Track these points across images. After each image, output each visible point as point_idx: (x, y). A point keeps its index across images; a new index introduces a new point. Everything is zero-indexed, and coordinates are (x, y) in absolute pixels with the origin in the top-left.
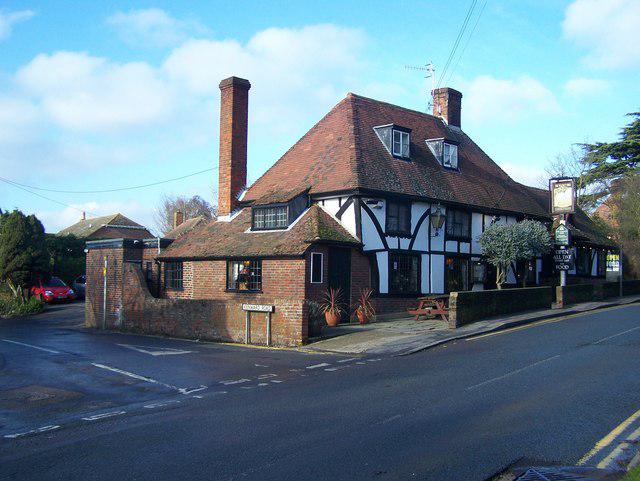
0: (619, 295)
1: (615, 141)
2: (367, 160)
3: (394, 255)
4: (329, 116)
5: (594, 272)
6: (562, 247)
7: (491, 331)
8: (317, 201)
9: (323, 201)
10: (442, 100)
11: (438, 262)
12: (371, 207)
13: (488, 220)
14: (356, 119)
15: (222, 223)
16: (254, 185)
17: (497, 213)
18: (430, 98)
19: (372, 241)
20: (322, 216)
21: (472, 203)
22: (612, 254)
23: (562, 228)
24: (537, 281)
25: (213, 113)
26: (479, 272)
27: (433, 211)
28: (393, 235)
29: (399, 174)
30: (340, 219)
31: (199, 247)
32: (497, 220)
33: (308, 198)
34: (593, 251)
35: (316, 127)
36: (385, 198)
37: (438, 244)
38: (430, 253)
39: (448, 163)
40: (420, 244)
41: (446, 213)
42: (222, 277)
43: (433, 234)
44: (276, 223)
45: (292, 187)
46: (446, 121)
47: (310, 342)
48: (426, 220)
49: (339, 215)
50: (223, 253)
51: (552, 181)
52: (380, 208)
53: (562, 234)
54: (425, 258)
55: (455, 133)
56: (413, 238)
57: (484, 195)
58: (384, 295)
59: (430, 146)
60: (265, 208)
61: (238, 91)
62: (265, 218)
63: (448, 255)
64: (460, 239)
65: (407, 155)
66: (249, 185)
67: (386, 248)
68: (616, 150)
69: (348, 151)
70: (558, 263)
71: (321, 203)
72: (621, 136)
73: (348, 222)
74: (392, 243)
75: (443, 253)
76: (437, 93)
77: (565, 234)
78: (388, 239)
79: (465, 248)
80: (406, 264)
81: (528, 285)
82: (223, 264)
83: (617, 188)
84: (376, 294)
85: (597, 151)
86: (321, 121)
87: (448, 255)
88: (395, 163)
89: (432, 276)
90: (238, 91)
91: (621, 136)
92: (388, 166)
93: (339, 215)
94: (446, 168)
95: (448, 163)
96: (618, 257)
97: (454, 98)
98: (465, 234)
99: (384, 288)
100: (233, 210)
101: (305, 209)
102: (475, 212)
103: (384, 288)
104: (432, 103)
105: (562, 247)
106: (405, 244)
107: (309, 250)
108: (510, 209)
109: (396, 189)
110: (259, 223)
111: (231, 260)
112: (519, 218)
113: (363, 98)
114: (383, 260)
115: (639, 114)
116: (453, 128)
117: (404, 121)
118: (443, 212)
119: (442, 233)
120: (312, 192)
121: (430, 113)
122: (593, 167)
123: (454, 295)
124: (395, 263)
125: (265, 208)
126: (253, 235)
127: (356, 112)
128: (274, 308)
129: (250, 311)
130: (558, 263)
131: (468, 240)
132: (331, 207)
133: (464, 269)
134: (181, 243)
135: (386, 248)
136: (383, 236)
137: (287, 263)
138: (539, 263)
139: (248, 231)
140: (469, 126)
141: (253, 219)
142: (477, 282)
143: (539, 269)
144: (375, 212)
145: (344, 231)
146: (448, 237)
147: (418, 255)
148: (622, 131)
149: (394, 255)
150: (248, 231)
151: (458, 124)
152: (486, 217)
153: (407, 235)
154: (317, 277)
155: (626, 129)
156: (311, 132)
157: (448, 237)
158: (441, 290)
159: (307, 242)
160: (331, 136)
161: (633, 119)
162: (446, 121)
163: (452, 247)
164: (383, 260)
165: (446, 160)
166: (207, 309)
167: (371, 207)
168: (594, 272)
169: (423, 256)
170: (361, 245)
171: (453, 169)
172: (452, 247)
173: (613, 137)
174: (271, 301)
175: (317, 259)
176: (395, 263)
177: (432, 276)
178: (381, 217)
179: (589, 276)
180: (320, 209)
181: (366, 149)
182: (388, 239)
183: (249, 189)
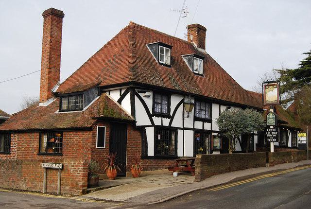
0: (125, 176)
1: (297, 68)
2: (140, 63)
3: (158, 129)
4: (117, 36)
5: (290, 145)
6: (271, 127)
7: (226, 183)
8: (105, 92)
9: (109, 92)
10: (193, 32)
11: (190, 135)
12: (142, 95)
13: (223, 108)
14: (134, 38)
15: (41, 107)
16: (65, 82)
17: (229, 104)
18: (186, 31)
19: (142, 119)
20: (108, 100)
21: (212, 96)
22: (300, 133)
23: (271, 114)
24: (255, 150)
25: (37, 27)
26: (217, 143)
27: (186, 101)
28: (158, 115)
29: (163, 75)
30: (120, 104)
31: (22, 124)
32: (228, 108)
33: (102, 89)
34: (289, 131)
35: (108, 44)
36: (152, 90)
37: (189, 123)
38: (184, 129)
39: (196, 70)
40: (177, 123)
41: (195, 102)
42: (36, 144)
43: (186, 115)
44: (76, 106)
45: (88, 81)
46: (195, 45)
47: (88, 192)
48: (182, 106)
49: (120, 101)
50: (37, 127)
51: (264, 84)
52: (148, 97)
53: (271, 120)
54: (180, 132)
55: (201, 53)
56: (172, 118)
57: (221, 92)
58: (151, 157)
59: (185, 60)
60: (68, 95)
61: (54, 17)
62: (69, 103)
63: (196, 132)
64: (204, 121)
65: (169, 63)
66: (61, 82)
67: (153, 125)
68: (297, 74)
69: (126, 60)
70: (269, 138)
71: (108, 93)
72: (300, 66)
73: (126, 105)
74: (157, 121)
75: (193, 129)
76: (190, 27)
77: (273, 118)
78: (154, 118)
79: (207, 126)
80: (166, 135)
81: (249, 152)
82: (37, 135)
83: (297, 97)
84: (145, 156)
85: (287, 74)
86: (112, 40)
87: (196, 132)
88: (160, 68)
89: (185, 146)
90: (54, 17)
91: (300, 66)
92: (155, 69)
93: (120, 101)
94: (194, 73)
95: (196, 70)
96: (305, 135)
97: (200, 31)
98: (207, 117)
99: (151, 152)
100: (48, 98)
101: (97, 97)
102: (214, 103)
103: (151, 152)
104: (187, 34)
105: (271, 127)
106: (166, 122)
107: (96, 124)
108: (237, 101)
109: (160, 84)
110: (65, 106)
111: (41, 132)
112: (243, 107)
113: (141, 26)
114: (150, 133)
115: (309, 53)
116: (200, 50)
117: (166, 42)
118: (193, 101)
119: (192, 115)
120: (102, 85)
121: (186, 40)
122: (285, 83)
123: (199, 156)
124: (159, 136)
125: (68, 95)
126: (60, 114)
127: (134, 33)
128: (63, 166)
129: (47, 169)
130: (269, 138)
131: (210, 121)
132: (115, 96)
133: (207, 140)
134: (12, 121)
135: (153, 125)
136: (150, 116)
137: (22, 127)
138: (256, 137)
139: (57, 112)
140: (210, 49)
141: (61, 103)
142: (217, 150)
143: (256, 141)
144: (145, 99)
145: (123, 112)
146: (196, 119)
147: (175, 130)
148: (301, 63)
149: (158, 129)
150: (57, 112)
151: (204, 48)
152: (222, 107)
153: (167, 116)
154: (101, 144)
155: (303, 62)
156: (105, 47)
157: (196, 119)
158: (191, 155)
159: (94, 118)
160: (117, 49)
161: (307, 56)
162: (195, 45)
163: (199, 125)
164: (150, 133)
165: (195, 68)
166: (19, 166)
167: (142, 95)
168: (290, 145)
169: (179, 131)
170: (135, 122)
171: (200, 75)
172: (199, 125)
173: (295, 65)
174: (62, 160)
175: (101, 131)
176: (159, 136)
177: (185, 146)
178: (149, 102)
179: (287, 147)
180: (107, 97)
181: (138, 58)
182: (154, 118)
183: (61, 85)
